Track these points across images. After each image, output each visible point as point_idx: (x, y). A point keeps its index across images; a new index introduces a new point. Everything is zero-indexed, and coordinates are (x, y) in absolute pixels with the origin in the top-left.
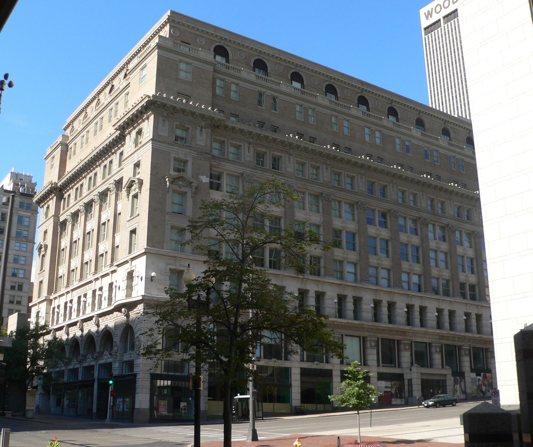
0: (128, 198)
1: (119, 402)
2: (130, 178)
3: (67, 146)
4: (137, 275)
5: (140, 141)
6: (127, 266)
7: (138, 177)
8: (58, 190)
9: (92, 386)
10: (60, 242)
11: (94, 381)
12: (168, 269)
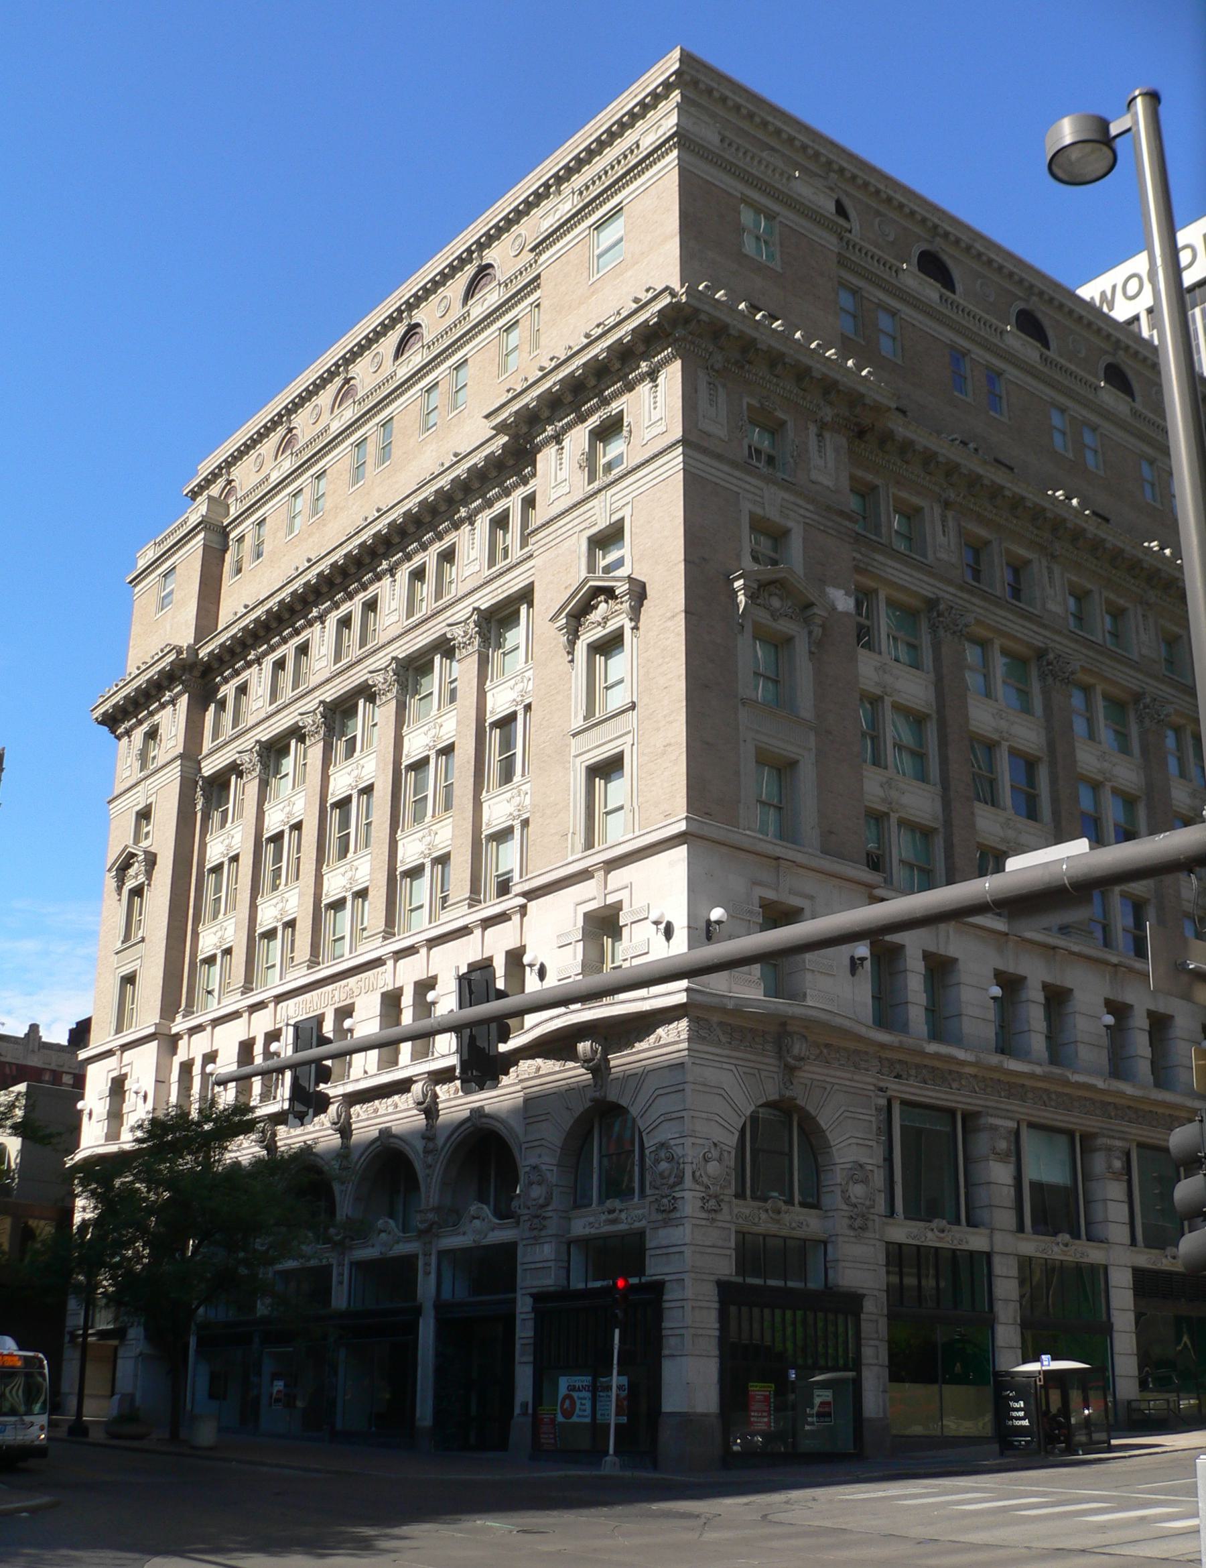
0: (120, 894)
1: (572, 1388)
2: (126, 847)
3: (224, 533)
4: (134, 1089)
5: (152, 754)
6: (111, 1062)
7: (144, 844)
8: (197, 673)
9: (412, 1329)
10: (203, 846)
11: (418, 1311)
12: (756, 902)
